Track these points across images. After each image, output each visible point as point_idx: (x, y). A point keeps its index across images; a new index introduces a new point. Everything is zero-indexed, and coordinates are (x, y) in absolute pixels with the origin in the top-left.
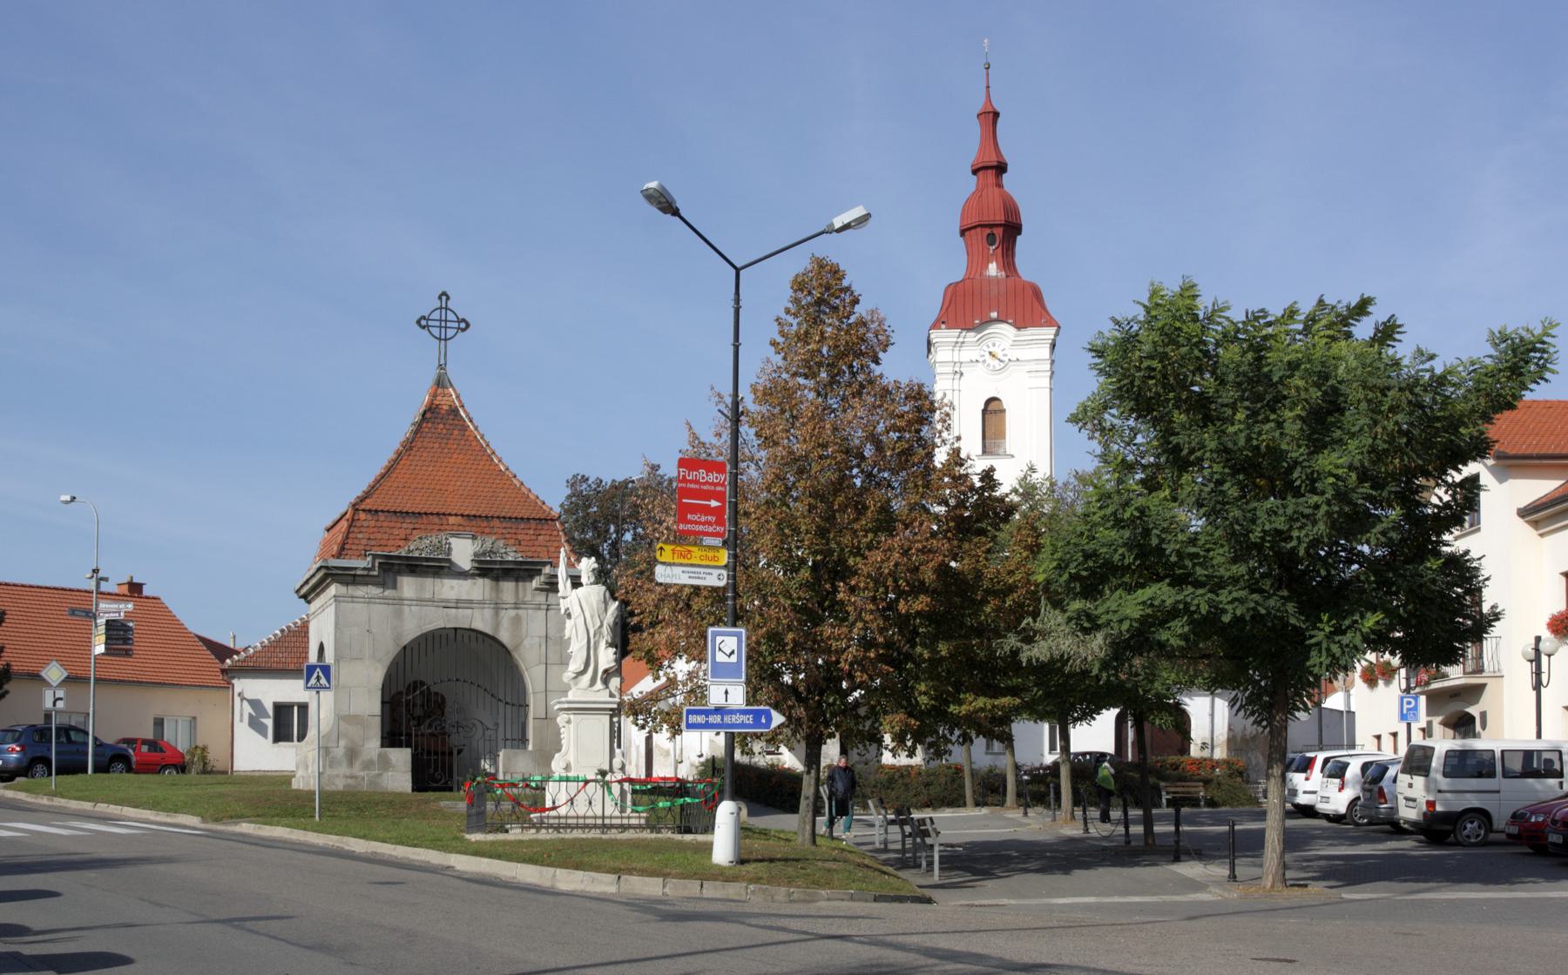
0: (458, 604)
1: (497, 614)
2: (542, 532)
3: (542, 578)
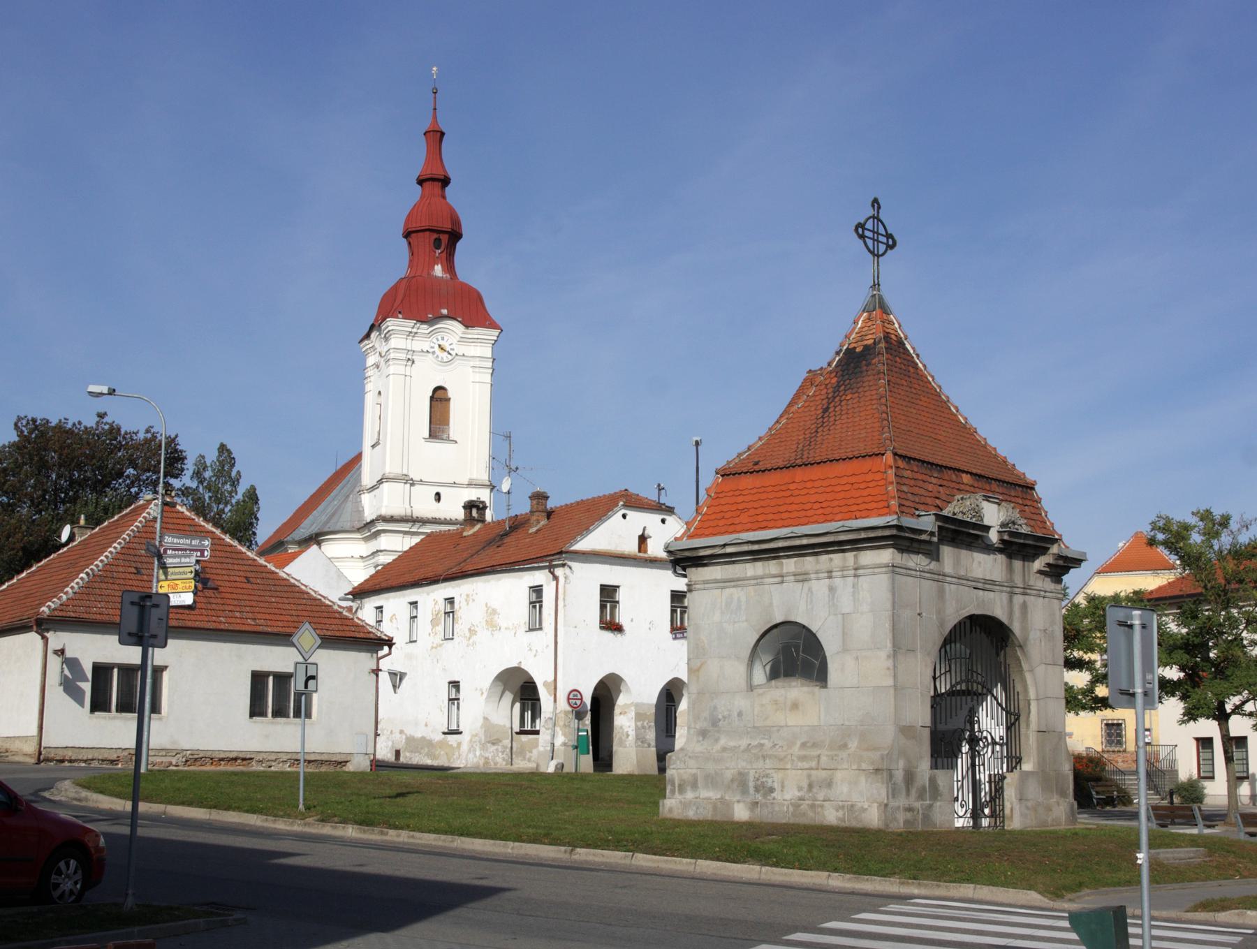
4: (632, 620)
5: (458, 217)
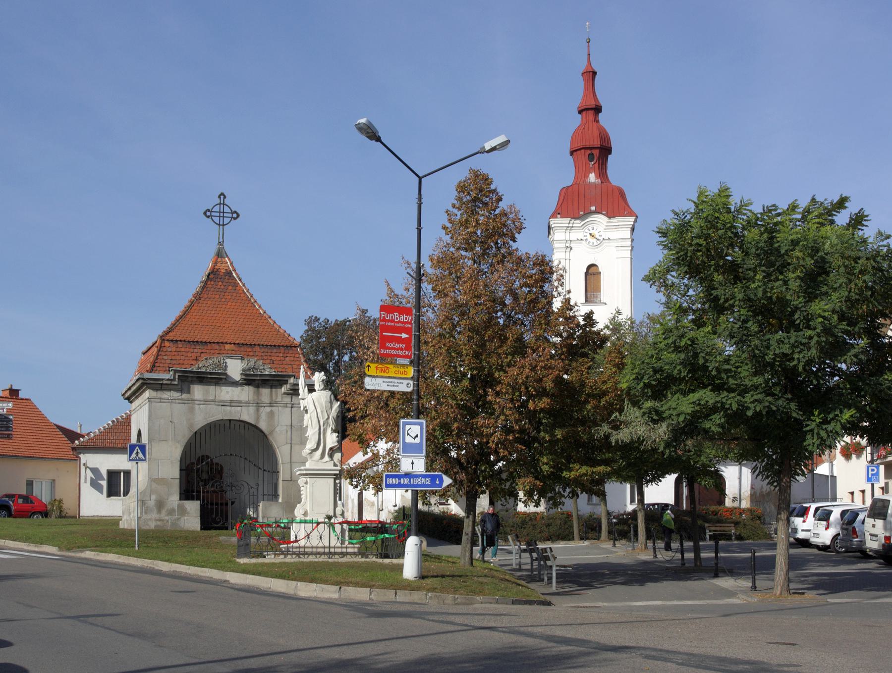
0: (232, 403)
1: (258, 410)
2: (288, 355)
3: (289, 386)
5: (605, 130)
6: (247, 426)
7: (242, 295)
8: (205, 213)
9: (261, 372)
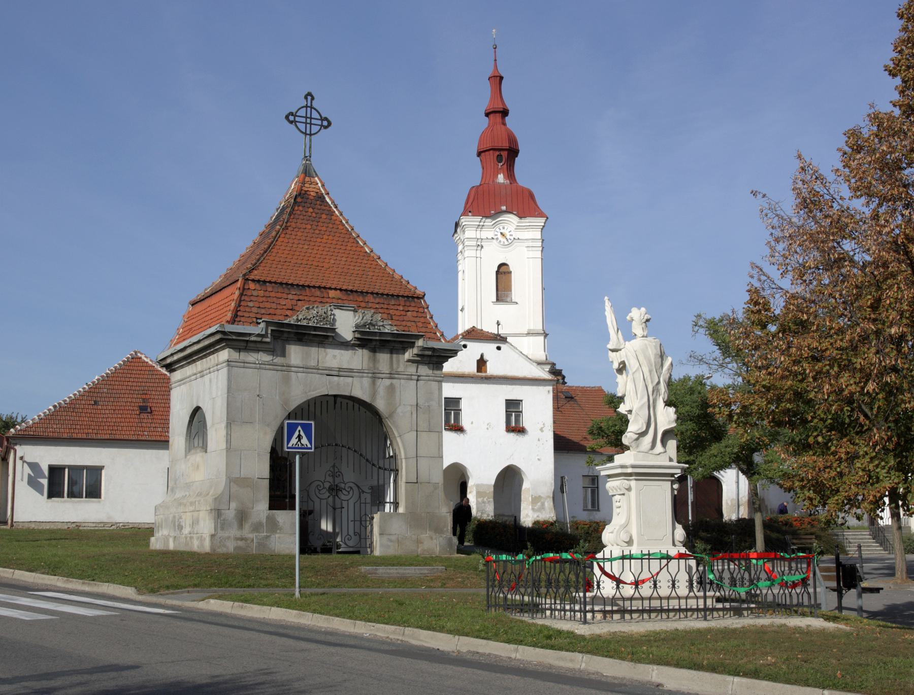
0: (341, 372)
1: (374, 383)
2: (411, 309)
3: (415, 351)
4: (472, 423)
5: (514, 136)
6: (351, 403)
7: (341, 227)
8: (287, 117)
9: (380, 330)
